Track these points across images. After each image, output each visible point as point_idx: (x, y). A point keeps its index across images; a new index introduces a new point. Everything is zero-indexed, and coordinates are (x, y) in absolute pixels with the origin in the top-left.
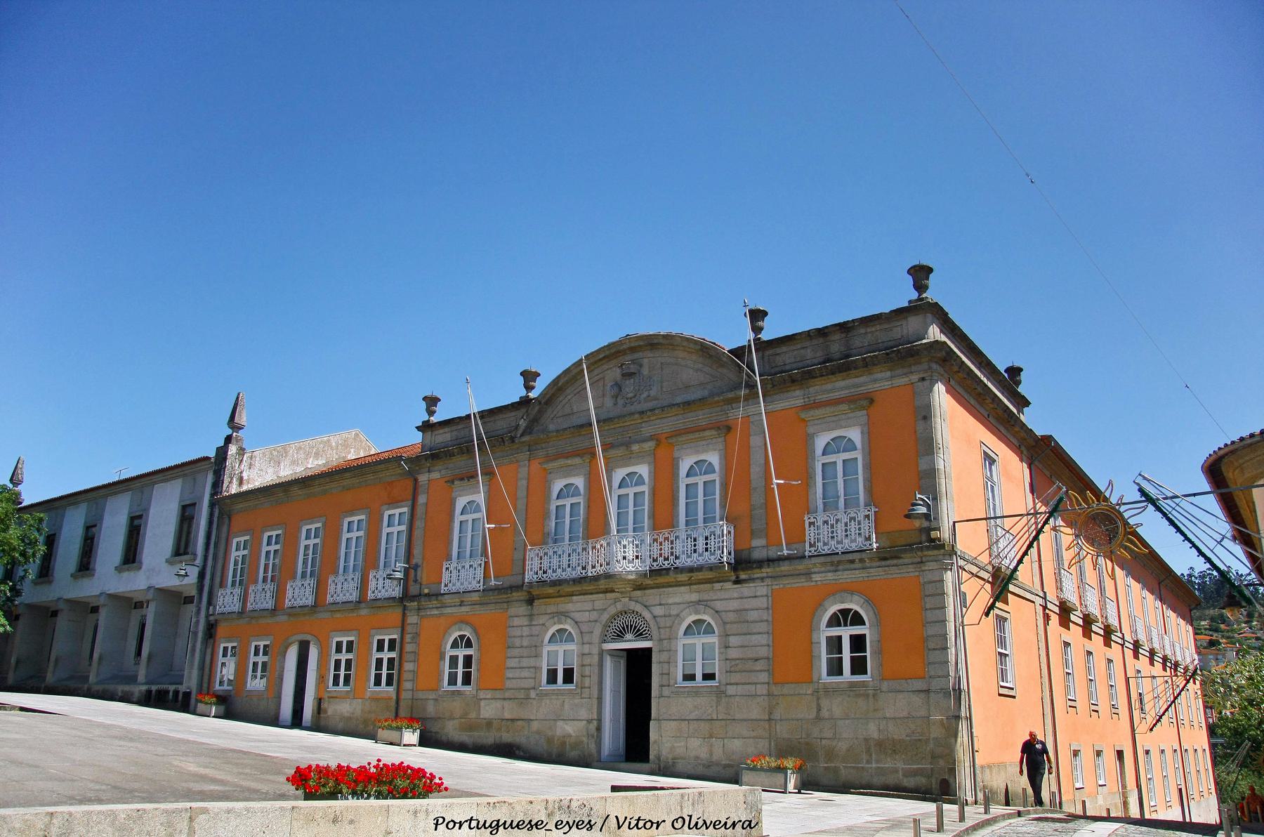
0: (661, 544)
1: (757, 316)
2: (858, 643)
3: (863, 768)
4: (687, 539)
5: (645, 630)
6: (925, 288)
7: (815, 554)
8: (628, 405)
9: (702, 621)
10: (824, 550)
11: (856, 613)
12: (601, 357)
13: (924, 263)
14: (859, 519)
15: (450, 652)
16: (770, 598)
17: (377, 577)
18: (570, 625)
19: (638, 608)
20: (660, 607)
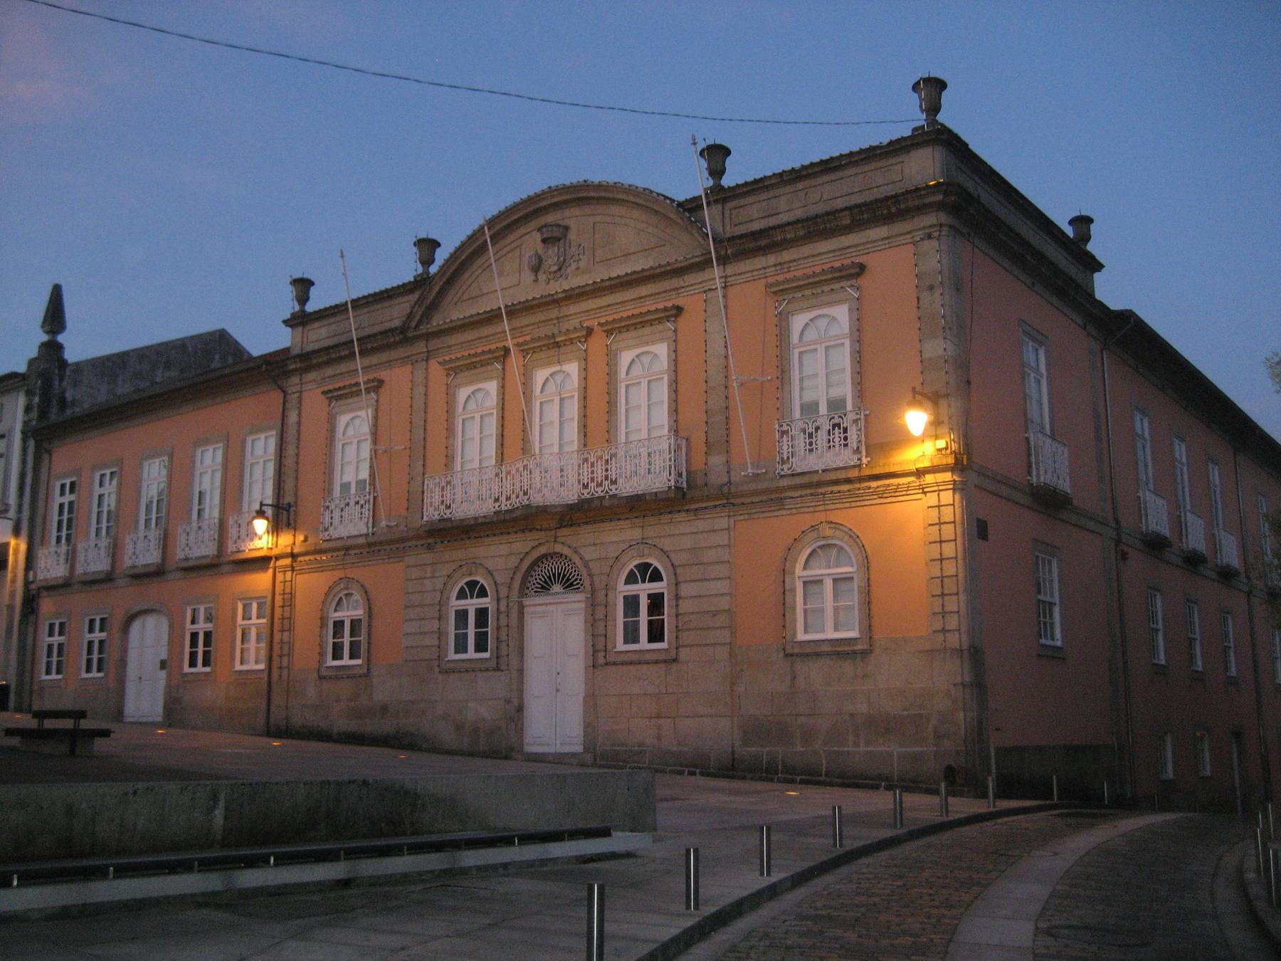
1: (716, 155)
3: (848, 752)
5: (576, 579)
7: (789, 472)
8: (552, 282)
9: (647, 565)
11: (656, 569)
14: (845, 425)
16: (732, 533)
18: (656, 558)
19: (566, 551)
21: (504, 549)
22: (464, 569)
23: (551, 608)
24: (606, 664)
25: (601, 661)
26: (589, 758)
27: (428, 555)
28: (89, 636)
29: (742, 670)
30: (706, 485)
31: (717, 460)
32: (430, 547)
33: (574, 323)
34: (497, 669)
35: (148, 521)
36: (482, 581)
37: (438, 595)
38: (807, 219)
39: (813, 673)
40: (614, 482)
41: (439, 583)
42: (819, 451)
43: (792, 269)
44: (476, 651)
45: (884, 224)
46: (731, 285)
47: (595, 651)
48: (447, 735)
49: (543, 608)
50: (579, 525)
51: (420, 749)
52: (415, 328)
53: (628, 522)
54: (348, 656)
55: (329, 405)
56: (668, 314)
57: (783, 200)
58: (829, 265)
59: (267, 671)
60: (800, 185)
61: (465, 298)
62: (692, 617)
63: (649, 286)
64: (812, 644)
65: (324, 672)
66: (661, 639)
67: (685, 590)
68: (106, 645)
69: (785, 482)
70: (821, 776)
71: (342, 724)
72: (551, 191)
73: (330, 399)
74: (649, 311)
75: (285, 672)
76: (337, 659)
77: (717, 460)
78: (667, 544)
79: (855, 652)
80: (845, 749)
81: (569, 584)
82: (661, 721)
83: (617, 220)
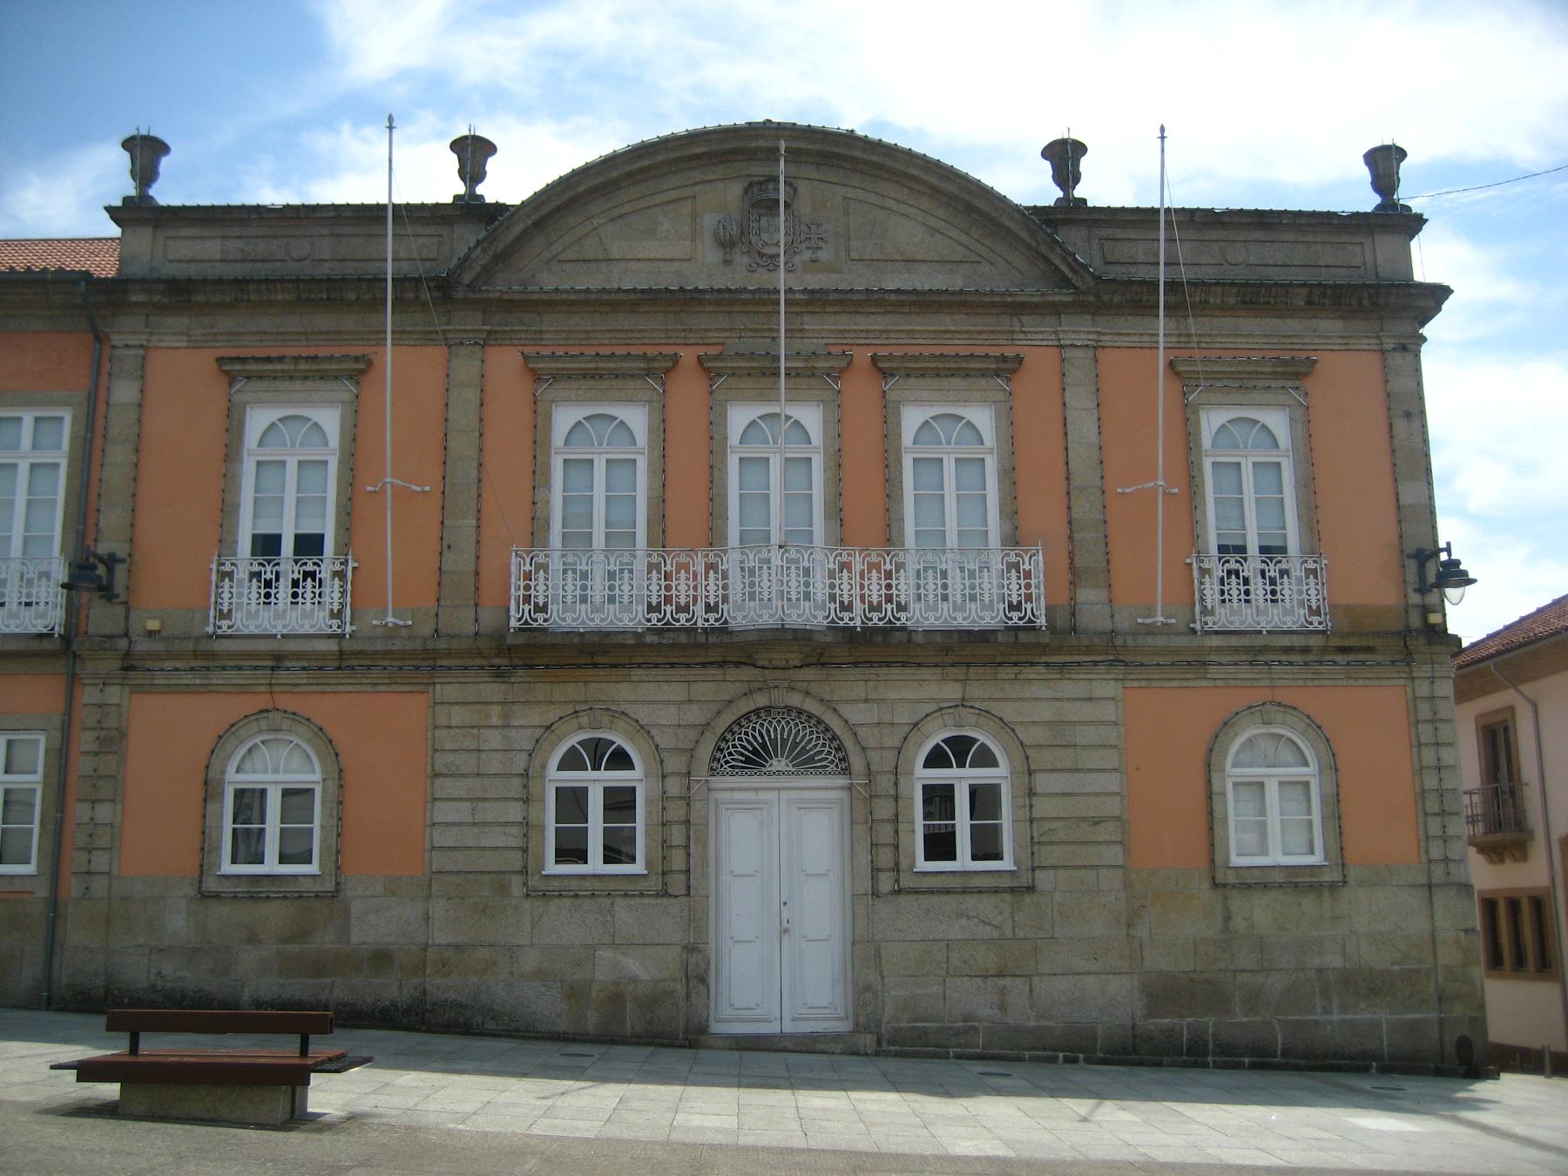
2: (620, 803)
3: (1316, 1022)
4: (565, 572)
7: (229, 632)
11: (984, 747)
12: (698, 151)
13: (156, 132)
15: (556, 777)
20: (867, 705)
21: (676, 692)
22: (584, 720)
23: (763, 795)
24: (899, 892)
26: (868, 1041)
27: (493, 686)
32: (499, 674)
38: (1246, 285)
39: (1259, 912)
40: (543, 609)
41: (523, 739)
42: (281, 605)
43: (1204, 345)
44: (557, 862)
45: (1340, 317)
48: (546, 1005)
49: (751, 795)
50: (838, 665)
51: (482, 1034)
53: (938, 670)
55: (230, 386)
56: (1003, 366)
58: (1275, 354)
60: (1212, 235)
61: (570, 257)
62: (1056, 824)
63: (958, 318)
64: (245, 878)
65: (211, 885)
67: (1043, 782)
69: (1216, 641)
70: (1275, 1056)
77: (1088, 596)
78: (1008, 711)
79: (1321, 884)
80: (1311, 1017)
82: (1007, 981)
83: (889, 203)
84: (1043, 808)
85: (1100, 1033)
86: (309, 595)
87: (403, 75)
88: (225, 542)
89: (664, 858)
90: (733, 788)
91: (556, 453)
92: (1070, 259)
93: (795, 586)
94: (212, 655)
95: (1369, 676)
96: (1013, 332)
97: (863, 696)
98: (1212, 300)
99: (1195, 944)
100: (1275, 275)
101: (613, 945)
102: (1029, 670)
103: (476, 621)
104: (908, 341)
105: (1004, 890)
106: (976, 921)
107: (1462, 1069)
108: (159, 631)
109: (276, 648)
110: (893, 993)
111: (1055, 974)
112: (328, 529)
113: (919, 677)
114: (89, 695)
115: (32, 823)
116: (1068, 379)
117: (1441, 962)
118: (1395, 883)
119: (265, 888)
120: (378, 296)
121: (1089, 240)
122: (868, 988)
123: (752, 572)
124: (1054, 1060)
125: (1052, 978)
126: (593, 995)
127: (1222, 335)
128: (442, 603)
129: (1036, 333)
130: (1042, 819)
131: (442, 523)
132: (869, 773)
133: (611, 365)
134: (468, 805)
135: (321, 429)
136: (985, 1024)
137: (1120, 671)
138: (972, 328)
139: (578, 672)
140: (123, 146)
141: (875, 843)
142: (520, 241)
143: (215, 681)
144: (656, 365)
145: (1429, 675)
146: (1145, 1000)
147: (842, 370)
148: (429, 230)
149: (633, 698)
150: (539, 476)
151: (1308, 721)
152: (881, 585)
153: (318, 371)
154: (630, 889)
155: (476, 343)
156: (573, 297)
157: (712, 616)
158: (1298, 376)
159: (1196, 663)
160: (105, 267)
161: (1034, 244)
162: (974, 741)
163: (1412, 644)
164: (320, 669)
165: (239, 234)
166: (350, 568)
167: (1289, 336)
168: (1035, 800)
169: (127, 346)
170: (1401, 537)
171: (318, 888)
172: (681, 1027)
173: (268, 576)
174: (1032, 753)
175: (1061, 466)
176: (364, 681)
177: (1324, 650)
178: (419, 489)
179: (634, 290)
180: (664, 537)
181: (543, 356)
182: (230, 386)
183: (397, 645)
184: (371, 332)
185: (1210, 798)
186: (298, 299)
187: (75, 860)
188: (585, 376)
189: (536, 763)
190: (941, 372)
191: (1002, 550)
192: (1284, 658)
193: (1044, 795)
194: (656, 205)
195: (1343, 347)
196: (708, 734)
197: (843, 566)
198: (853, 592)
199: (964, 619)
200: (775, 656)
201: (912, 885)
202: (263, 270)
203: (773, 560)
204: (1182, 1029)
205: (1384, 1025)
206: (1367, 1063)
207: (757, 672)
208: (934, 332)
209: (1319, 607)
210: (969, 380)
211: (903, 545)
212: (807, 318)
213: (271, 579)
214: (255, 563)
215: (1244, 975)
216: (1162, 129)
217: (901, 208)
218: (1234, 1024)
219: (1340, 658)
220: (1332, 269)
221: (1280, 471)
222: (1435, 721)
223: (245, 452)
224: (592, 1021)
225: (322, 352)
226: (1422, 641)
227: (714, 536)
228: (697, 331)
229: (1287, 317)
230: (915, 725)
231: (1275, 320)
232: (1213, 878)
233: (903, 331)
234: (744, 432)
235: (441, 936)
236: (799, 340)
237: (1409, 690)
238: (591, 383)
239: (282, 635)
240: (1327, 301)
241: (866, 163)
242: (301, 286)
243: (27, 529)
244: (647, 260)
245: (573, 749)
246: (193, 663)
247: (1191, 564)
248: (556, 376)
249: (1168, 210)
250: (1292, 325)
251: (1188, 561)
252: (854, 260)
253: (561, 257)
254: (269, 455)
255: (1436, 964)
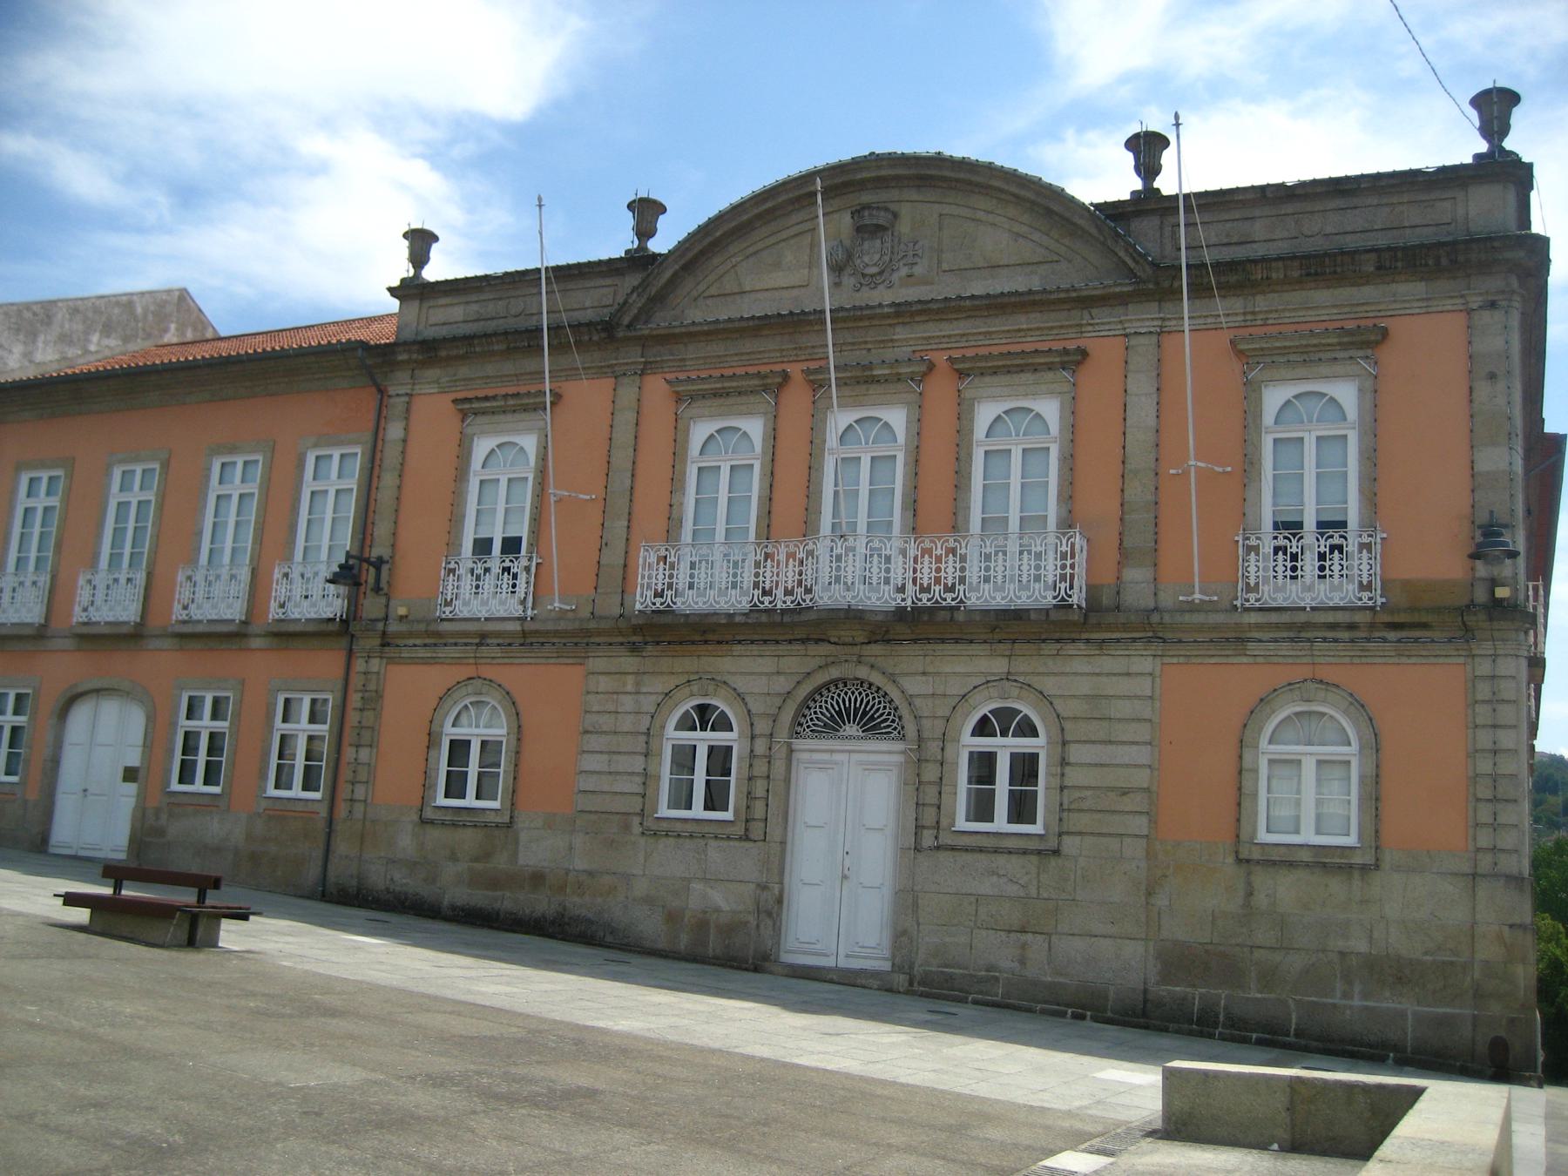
0: (939, 559)
3: (1334, 1006)
4: (1021, 553)
5: (886, 720)
6: (1504, 130)
7: (450, 616)
10: (1020, 598)
16: (1158, 680)
17: (93, 583)
19: (876, 679)
20: (924, 678)
21: (768, 664)
22: (695, 688)
23: (837, 757)
24: (938, 848)
25: (928, 839)
26: (901, 980)
27: (629, 659)
28: (222, 725)
29: (1165, 876)
30: (1118, 608)
31: (1136, 576)
32: (634, 649)
33: (903, 352)
34: (746, 838)
35: (115, 559)
36: (723, 707)
37: (646, 721)
39: (1284, 890)
41: (648, 704)
43: (1270, 322)
45: (1422, 279)
46: (1169, 332)
47: (919, 828)
48: (650, 926)
49: (826, 756)
50: (900, 641)
51: (601, 944)
52: (628, 326)
53: (987, 646)
54: (202, 780)
55: (463, 421)
56: (1066, 359)
57: (1258, 225)
58: (1339, 324)
59: (326, 803)
60: (1289, 208)
62: (1088, 793)
63: (1032, 316)
65: (429, 814)
66: (15, 774)
67: (1076, 753)
68: (25, 737)
69: (1253, 618)
70: (1288, 1035)
71: (457, 894)
72: (875, 160)
73: (464, 415)
74: (1036, 351)
75: (359, 808)
76: (713, 809)
77: (1136, 576)
78: (1049, 685)
79: (1351, 866)
80: (1330, 1001)
81: (872, 724)
82: (1029, 937)
84: (1074, 777)
85: (1112, 995)
86: (1336, 568)
87: (1125, 79)
88: (453, 545)
89: (748, 807)
90: (807, 747)
91: (1266, 433)
92: (1131, 251)
93: (876, 573)
94: (438, 634)
95: (1424, 653)
96: (1081, 325)
97: (921, 670)
98: (1274, 275)
99: (1213, 916)
100: (1351, 242)
101: (705, 880)
102: (1070, 646)
103: (622, 604)
104: (987, 342)
105: (1032, 852)
106: (1005, 880)
107: (1490, 1072)
108: (406, 616)
109: (478, 628)
110: (927, 939)
111: (1073, 935)
112: (523, 530)
113: (970, 653)
114: (359, 665)
115: (322, 761)
116: (1131, 367)
117: (1480, 956)
118: (1435, 870)
119: (465, 817)
120: (563, 340)
121: (1161, 228)
122: (904, 932)
123: (839, 558)
124: (1063, 1015)
125: (1070, 937)
126: (686, 920)
127: (1289, 310)
128: (599, 590)
129: (1102, 324)
130: (1074, 787)
131: (603, 525)
132: (920, 739)
133: (735, 384)
134: (605, 757)
135: (891, 427)
136: (1005, 975)
137: (1157, 648)
138: (1042, 325)
139: (694, 647)
140: (666, 210)
141: (921, 802)
142: (673, 282)
143: (440, 655)
144: (769, 381)
145: (1491, 652)
146: (1159, 966)
147: (925, 375)
148: (608, 281)
149: (733, 670)
150: (676, 482)
151: (1350, 699)
152: (880, 569)
153: (522, 405)
154: (718, 832)
155: (636, 373)
156: (706, 328)
157: (789, 599)
158: (1367, 344)
159: (1237, 640)
160: (384, 335)
161: (1102, 239)
162: (718, 708)
163: (1470, 620)
164: (510, 645)
165: (477, 299)
166: (534, 564)
167: (1363, 304)
168: (1068, 770)
169: (398, 395)
170: (1473, 506)
171: (498, 820)
172: (751, 952)
173: (1294, 550)
174: (1068, 726)
175: (1119, 451)
176: (539, 655)
177: (1372, 626)
178: (1220, 470)
179: (753, 318)
180: (769, 532)
181: (681, 381)
182: (463, 421)
183: (562, 626)
184: (562, 370)
185: (1240, 772)
186: (508, 348)
187: (344, 791)
188: (715, 395)
189: (657, 722)
190: (1011, 369)
191: (868, 537)
192: (1330, 634)
193: (1077, 764)
194: (784, 240)
195: (1424, 310)
196: (789, 702)
197: (767, 556)
198: (907, 575)
199: (978, 599)
200: (843, 633)
201: (950, 842)
202: (491, 326)
203: (857, 549)
204: (1194, 999)
205: (1410, 1017)
206: (1384, 1053)
207: (832, 647)
208: (1008, 331)
209: (1370, 582)
210: (1038, 375)
211: (968, 531)
212: (899, 329)
213: (1297, 553)
214: (1365, 535)
215: (1261, 950)
216: (540, 199)
217: (991, 218)
218: (1248, 999)
219: (1392, 635)
220: (1418, 229)
221: (343, 490)
222: (1495, 701)
223: (471, 474)
224: (684, 941)
225: (523, 390)
226: (1482, 616)
227: (808, 527)
228: (806, 348)
229: (1363, 285)
230: (964, 696)
231: (1348, 289)
232: (1237, 852)
233: (980, 333)
234: (990, 428)
235: (580, 864)
236: (891, 350)
237: (1469, 668)
238: (721, 401)
239: (1311, 608)
240: (1399, 264)
241: (957, 180)
242: (509, 337)
243: (331, 540)
244: (773, 289)
245: (687, 713)
246: (428, 641)
247: (1238, 541)
248: (693, 397)
249: (1187, 196)
250: (1367, 292)
251: (1236, 538)
252: (945, 271)
253: (706, 294)
254: (997, 444)
255: (1473, 958)
